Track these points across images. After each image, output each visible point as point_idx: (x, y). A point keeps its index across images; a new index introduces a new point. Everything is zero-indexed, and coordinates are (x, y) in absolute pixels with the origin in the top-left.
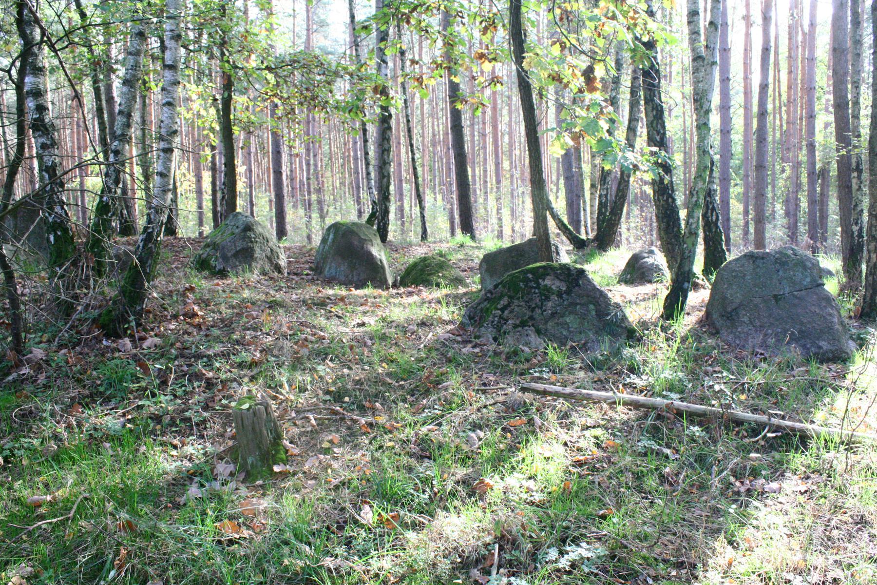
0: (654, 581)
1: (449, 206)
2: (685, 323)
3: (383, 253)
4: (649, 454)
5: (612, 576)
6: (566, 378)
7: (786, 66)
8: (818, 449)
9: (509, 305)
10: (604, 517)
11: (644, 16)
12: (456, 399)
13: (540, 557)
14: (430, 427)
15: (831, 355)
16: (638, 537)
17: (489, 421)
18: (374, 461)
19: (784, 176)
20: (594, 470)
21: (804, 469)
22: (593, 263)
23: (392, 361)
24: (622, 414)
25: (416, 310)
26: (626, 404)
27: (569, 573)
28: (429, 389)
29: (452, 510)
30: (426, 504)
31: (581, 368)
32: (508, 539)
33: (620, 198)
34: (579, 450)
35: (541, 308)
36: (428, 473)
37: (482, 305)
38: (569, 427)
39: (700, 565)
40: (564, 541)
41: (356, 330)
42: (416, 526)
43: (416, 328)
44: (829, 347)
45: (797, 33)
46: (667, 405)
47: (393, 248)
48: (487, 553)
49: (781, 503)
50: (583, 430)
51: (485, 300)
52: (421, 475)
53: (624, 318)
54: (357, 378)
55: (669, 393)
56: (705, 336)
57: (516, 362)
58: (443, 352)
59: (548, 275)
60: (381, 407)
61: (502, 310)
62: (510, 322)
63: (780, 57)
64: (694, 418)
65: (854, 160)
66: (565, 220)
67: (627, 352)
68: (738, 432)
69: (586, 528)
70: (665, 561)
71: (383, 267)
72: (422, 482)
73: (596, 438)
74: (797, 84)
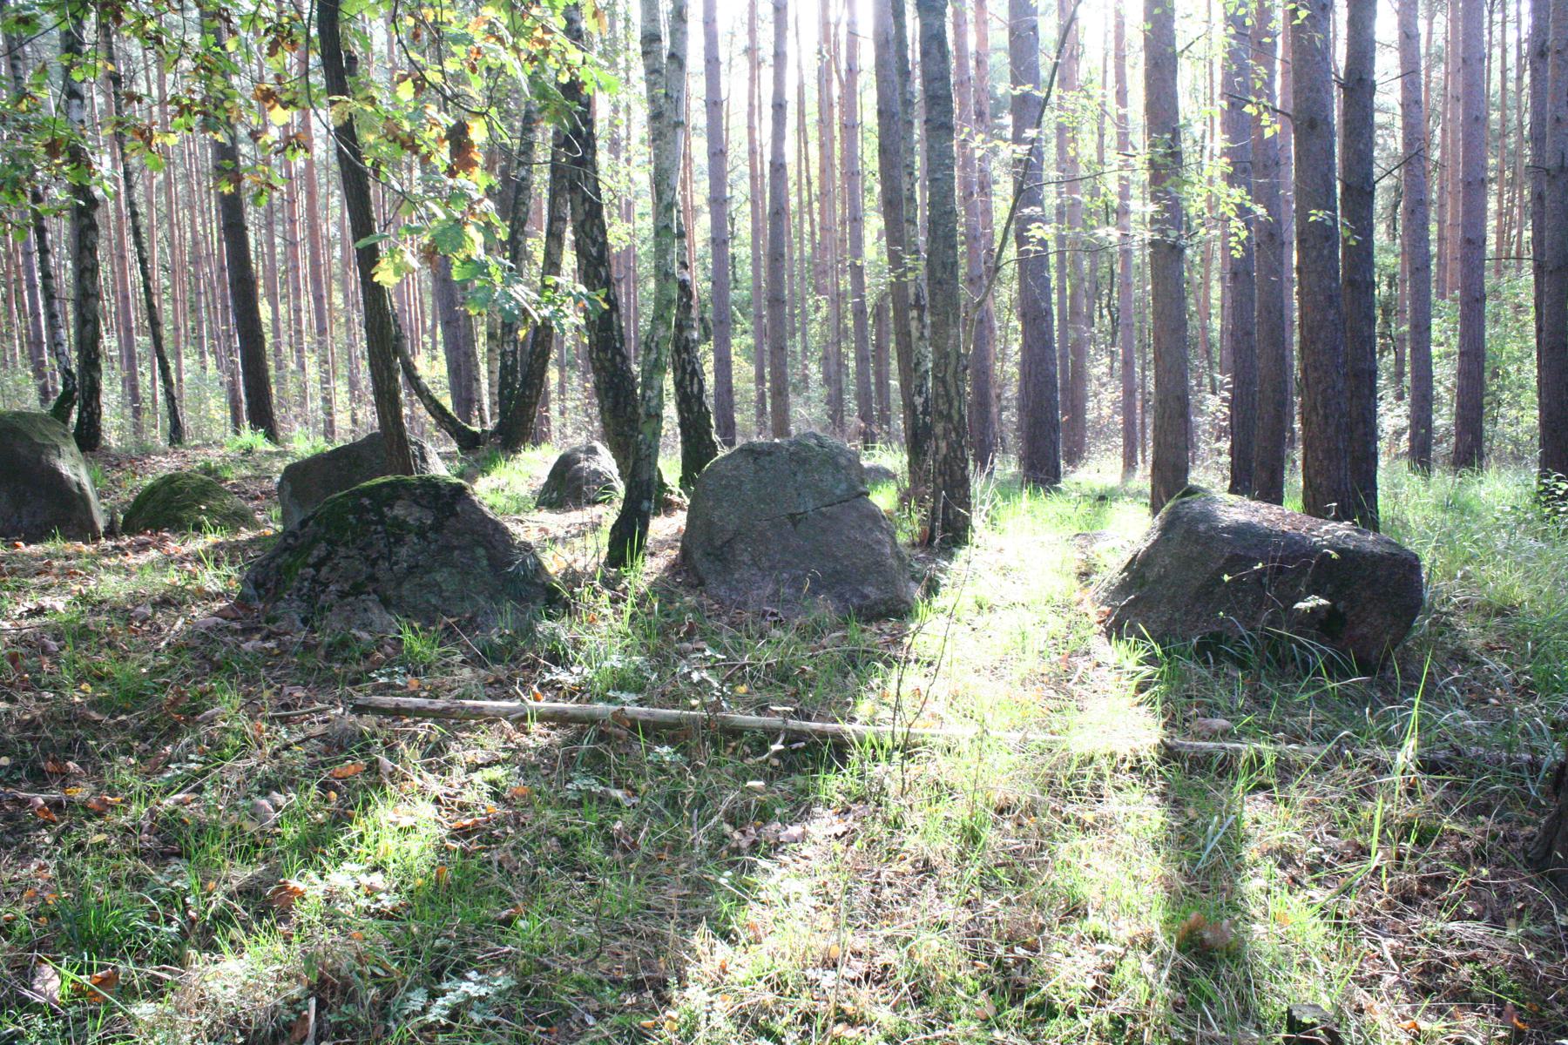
0: (597, 1019)
1: (227, 379)
2: (647, 571)
3: (82, 471)
4: (586, 802)
5: (526, 1022)
6: (437, 682)
7: (817, 134)
8: (862, 761)
9: (328, 557)
10: (508, 922)
11: (560, 37)
12: (230, 739)
13: (394, 1009)
14: (180, 796)
15: (883, 608)
16: (569, 948)
17: (293, 772)
18: (63, 875)
20: (490, 840)
22: (494, 474)
23: (101, 679)
24: (538, 736)
25: (149, 575)
26: (542, 718)
27: (449, 1028)
28: (176, 724)
29: (226, 948)
30: (173, 944)
31: (463, 661)
32: (333, 986)
34: (463, 807)
35: (389, 560)
36: (176, 884)
37: (280, 561)
38: (443, 770)
39: (672, 980)
40: (438, 975)
41: (25, 623)
42: (156, 990)
43: (150, 611)
46: (614, 714)
47: (116, 461)
48: (293, 1017)
49: (805, 858)
50: (468, 772)
51: (285, 550)
52: (163, 890)
53: (539, 565)
54: (27, 717)
56: (681, 590)
57: (345, 661)
58: (204, 653)
59: (399, 498)
60: (79, 769)
61: (317, 566)
62: (332, 587)
63: (807, 120)
64: (656, 731)
65: (912, 291)
66: (447, 402)
67: (545, 626)
68: (735, 749)
69: (475, 944)
70: (616, 982)
71: (84, 498)
72: (164, 902)
73: (493, 783)
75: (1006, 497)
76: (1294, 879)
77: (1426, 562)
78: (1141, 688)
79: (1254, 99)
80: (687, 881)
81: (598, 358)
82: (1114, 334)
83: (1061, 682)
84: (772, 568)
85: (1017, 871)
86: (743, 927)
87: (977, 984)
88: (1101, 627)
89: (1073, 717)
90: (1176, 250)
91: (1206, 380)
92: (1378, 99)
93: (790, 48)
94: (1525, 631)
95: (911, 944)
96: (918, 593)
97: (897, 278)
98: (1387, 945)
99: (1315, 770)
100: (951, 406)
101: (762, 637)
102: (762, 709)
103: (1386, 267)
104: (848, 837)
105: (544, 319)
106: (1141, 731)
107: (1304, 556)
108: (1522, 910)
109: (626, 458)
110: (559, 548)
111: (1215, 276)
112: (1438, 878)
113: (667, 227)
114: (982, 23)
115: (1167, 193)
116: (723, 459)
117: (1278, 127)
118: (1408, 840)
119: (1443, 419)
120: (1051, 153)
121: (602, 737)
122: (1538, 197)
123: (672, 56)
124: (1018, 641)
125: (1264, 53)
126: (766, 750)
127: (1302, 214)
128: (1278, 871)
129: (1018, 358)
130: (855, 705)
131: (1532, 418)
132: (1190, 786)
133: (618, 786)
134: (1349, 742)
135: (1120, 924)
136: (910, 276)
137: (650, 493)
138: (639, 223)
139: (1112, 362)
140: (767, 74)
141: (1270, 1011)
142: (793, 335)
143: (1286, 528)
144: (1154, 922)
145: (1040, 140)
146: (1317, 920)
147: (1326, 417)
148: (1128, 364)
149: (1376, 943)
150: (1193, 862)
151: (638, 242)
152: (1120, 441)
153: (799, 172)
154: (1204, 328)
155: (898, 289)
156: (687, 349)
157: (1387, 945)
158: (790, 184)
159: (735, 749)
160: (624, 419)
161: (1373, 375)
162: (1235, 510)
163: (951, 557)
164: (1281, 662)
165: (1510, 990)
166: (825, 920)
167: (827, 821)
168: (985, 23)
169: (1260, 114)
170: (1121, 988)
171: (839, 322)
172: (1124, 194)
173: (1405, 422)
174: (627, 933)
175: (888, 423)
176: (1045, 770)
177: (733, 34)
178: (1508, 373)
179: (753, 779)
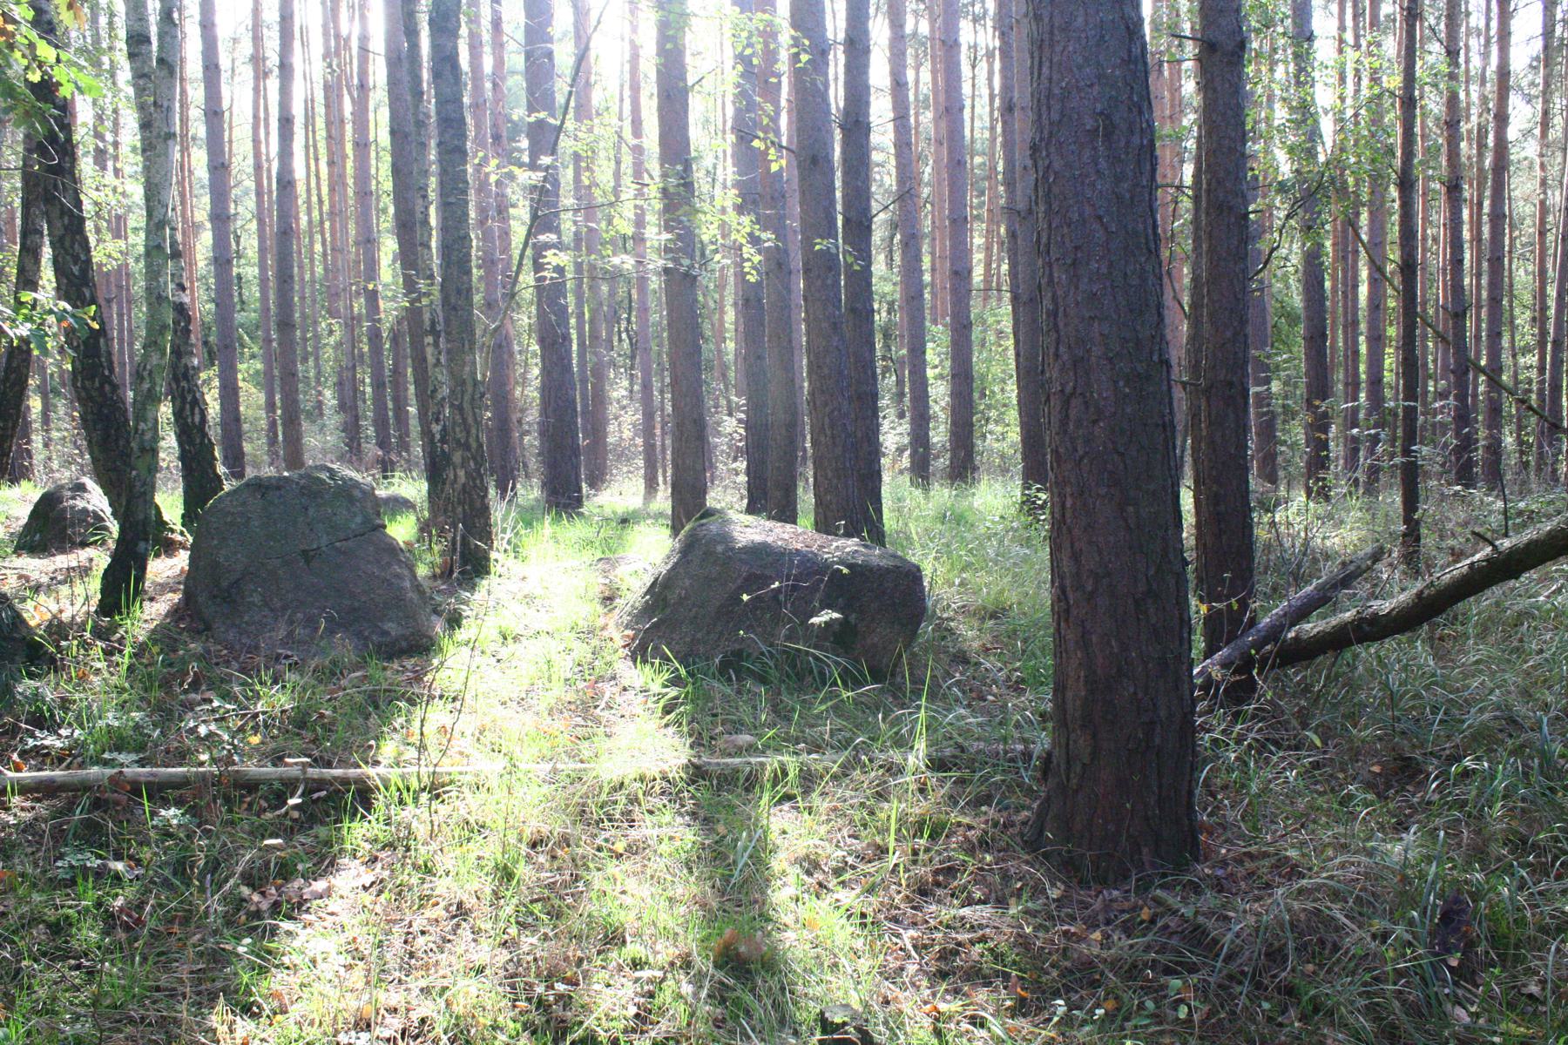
2: (148, 616)
8: (387, 807)
15: (404, 644)
19: (332, 340)
21: (368, 846)
33: (13, 385)
44: (401, 631)
45: (340, 96)
46: (111, 778)
49: (332, 914)
55: (115, 755)
64: (160, 792)
65: (427, 316)
67: (25, 686)
74: (345, 185)
75: (529, 524)
76: (820, 885)
77: (927, 571)
78: (667, 710)
79: (761, 135)
80: (201, 954)
81: (84, 387)
82: (633, 357)
83: (587, 708)
84: (284, 608)
85: (552, 905)
86: (266, 997)
87: (519, 1026)
88: (626, 651)
89: (601, 743)
90: (690, 280)
91: (723, 402)
92: (875, 138)
93: (297, 60)
94: (1015, 631)
95: (448, 993)
96: (439, 627)
97: (412, 302)
98: (909, 935)
99: (835, 777)
100: (468, 432)
101: (275, 682)
102: (278, 760)
103: (884, 296)
104: (378, 886)
105: (21, 339)
106: (667, 751)
107: (817, 573)
108: (1021, 889)
109: (119, 495)
110: (42, 598)
111: (729, 300)
112: (949, 868)
113: (159, 247)
114: (498, 46)
115: (680, 222)
116: (228, 494)
117: (784, 162)
118: (922, 837)
119: (939, 435)
120: (567, 176)
121: (97, 804)
122: (1012, 235)
123: (161, 61)
124: (539, 672)
125: (772, 92)
126: (285, 803)
127: (808, 244)
128: (805, 877)
129: (537, 383)
130: (378, 747)
131: (1015, 435)
132: (719, 803)
133: (118, 857)
134: (865, 748)
135: (658, 947)
136: (425, 301)
137: (146, 533)
138: (132, 239)
139: (632, 384)
140: (273, 85)
141: (805, 1014)
142: (305, 360)
143: (799, 546)
144: (690, 942)
145: (556, 168)
146: (844, 920)
147: (833, 437)
148: (646, 387)
149: (898, 936)
150: (726, 879)
151: (131, 261)
152: (641, 463)
153: (309, 191)
154: (720, 351)
155: (413, 314)
156: (186, 376)
157: (909, 935)
158: (300, 202)
159: (250, 805)
160: (117, 452)
161: (875, 397)
162: (750, 530)
163: (472, 588)
164: (801, 676)
165: (1014, 963)
166: (357, 977)
167: (353, 872)
168: (502, 45)
169: (767, 148)
170: (662, 1011)
171: (354, 347)
172: (640, 223)
173: (906, 440)
174: (131, 1021)
175: (407, 451)
176: (576, 799)
177: (235, 41)
178: (993, 392)
179: (271, 836)
